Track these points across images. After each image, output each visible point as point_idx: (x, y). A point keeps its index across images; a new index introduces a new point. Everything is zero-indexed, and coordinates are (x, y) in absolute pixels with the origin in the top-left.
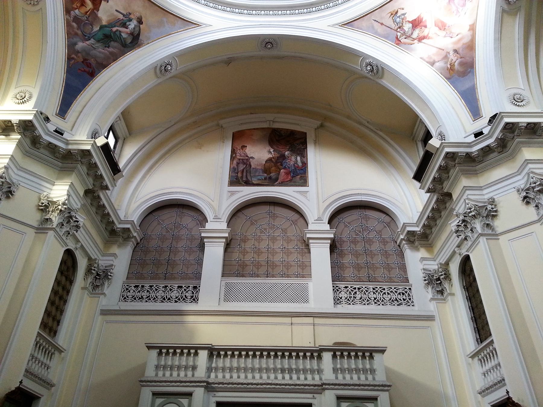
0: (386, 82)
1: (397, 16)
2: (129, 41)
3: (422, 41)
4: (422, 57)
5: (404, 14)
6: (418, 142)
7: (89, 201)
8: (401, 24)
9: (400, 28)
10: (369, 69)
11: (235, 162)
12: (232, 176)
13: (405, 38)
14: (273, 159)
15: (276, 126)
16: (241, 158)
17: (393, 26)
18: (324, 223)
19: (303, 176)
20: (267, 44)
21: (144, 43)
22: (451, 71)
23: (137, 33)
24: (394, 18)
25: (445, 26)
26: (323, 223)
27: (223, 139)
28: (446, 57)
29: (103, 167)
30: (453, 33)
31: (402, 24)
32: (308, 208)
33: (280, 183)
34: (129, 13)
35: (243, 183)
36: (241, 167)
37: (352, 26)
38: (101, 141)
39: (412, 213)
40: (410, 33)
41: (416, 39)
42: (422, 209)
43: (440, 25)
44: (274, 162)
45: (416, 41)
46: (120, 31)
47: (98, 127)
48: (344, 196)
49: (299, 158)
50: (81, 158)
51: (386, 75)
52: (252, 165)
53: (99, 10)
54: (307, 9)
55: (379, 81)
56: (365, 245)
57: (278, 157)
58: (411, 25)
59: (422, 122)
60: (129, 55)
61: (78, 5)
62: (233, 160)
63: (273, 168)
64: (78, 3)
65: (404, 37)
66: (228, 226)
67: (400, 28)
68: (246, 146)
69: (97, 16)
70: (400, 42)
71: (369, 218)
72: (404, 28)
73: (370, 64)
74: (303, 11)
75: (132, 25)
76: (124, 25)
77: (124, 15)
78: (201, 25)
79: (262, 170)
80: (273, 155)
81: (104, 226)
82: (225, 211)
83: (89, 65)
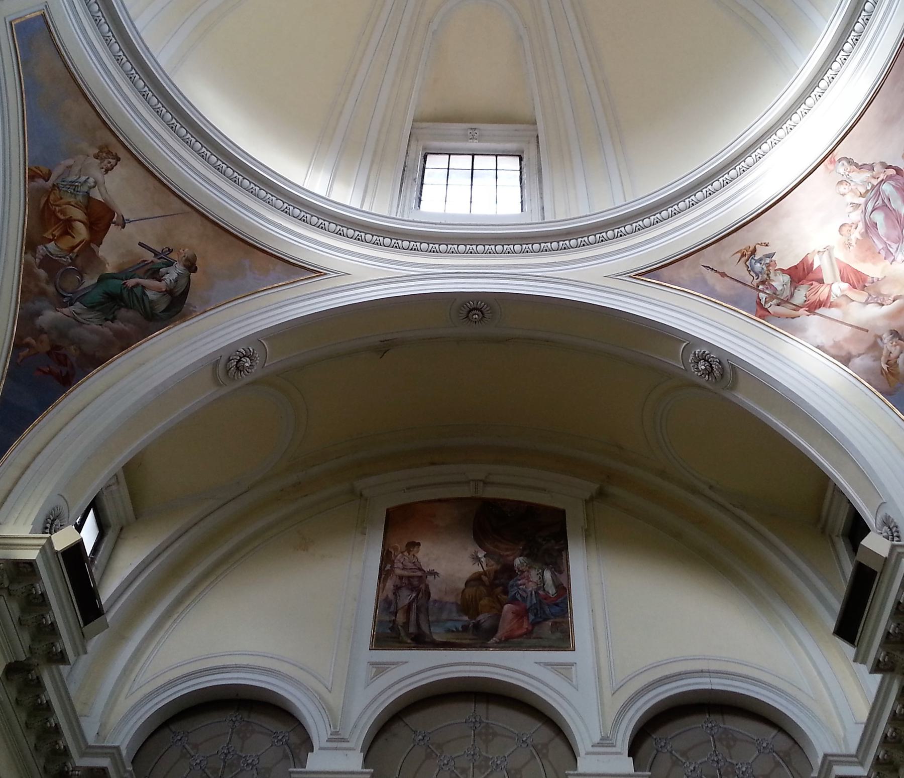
0: (743, 398)
1: (756, 258)
2: (163, 307)
3: (817, 311)
4: (820, 345)
5: (770, 256)
6: (836, 539)
7: (14, 694)
8: (765, 276)
9: (763, 283)
10: (703, 367)
11: (390, 584)
12: (381, 622)
13: (778, 305)
14: (484, 577)
15: (491, 493)
16: (406, 573)
17: (748, 279)
18: (620, 753)
19: (560, 623)
21: (195, 311)
22: (891, 378)
23: (179, 290)
24: (748, 263)
25: (864, 280)
26: (617, 753)
27: (361, 526)
28: (875, 347)
29: (62, 607)
30: (884, 295)
32: (580, 717)
33: (501, 641)
34: (169, 249)
35: (409, 641)
36: (406, 597)
38: (63, 540)
39: (844, 728)
40: (787, 293)
41: (802, 308)
42: (867, 714)
43: (853, 278)
44: (487, 583)
46: (144, 287)
47: (61, 503)
48: (667, 677)
49: (548, 575)
50: (11, 582)
52: (432, 590)
53: (101, 243)
54: (558, 242)
55: (727, 394)
56: (715, 747)
57: (496, 572)
58: (787, 278)
59: (839, 492)
60: (159, 337)
61: (57, 233)
62: (385, 580)
63: (485, 602)
64: (56, 229)
65: (775, 301)
66: (366, 762)
67: (763, 283)
68: (419, 544)
69: (94, 254)
70: (767, 313)
71: (735, 740)
72: (773, 284)
73: (704, 358)
74: (549, 246)
75: (171, 275)
76: (155, 274)
77: (156, 254)
78: (325, 274)
79: (457, 604)
80: (484, 565)
81: (42, 762)
82: (360, 718)
83: (62, 360)
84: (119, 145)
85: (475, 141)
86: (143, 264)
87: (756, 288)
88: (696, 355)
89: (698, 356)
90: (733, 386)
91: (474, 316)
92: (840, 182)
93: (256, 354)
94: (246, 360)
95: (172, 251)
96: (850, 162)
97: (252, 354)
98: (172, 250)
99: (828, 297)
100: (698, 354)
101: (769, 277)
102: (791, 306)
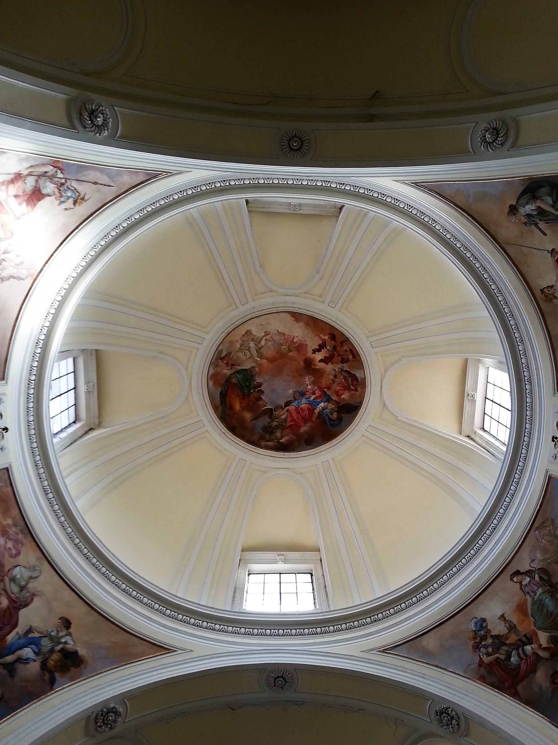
2: (544, 190)
5: (62, 202)
8: (62, 189)
9: (62, 184)
13: (46, 172)
17: (75, 184)
20: (301, 147)
23: (527, 196)
31: (60, 190)
34: (526, 224)
37: (148, 174)
40: (41, 182)
45: (25, 172)
51: (62, 112)
58: (44, 191)
70: (53, 165)
73: (100, 128)
75: (530, 208)
76: (541, 212)
77: (536, 225)
84: (539, 299)
85: (293, 203)
86: (548, 221)
87: (66, 180)
88: (106, 128)
89: (104, 127)
90: (69, 103)
91: (296, 144)
92: (22, 263)
93: (479, 141)
94: (488, 140)
95: (524, 223)
96: (19, 278)
97: (483, 143)
98: (523, 224)
99: (7, 188)
100: (105, 130)
101: (58, 189)
102: (35, 174)
